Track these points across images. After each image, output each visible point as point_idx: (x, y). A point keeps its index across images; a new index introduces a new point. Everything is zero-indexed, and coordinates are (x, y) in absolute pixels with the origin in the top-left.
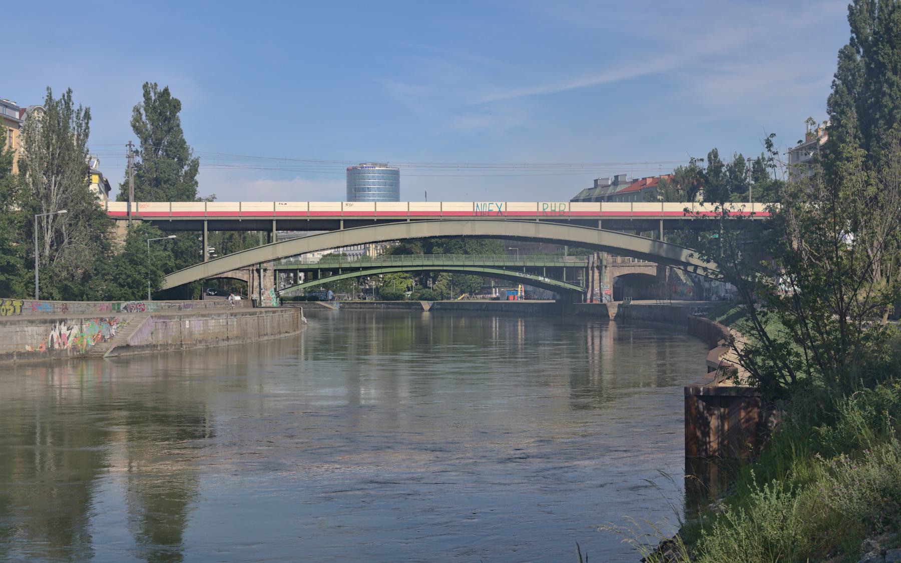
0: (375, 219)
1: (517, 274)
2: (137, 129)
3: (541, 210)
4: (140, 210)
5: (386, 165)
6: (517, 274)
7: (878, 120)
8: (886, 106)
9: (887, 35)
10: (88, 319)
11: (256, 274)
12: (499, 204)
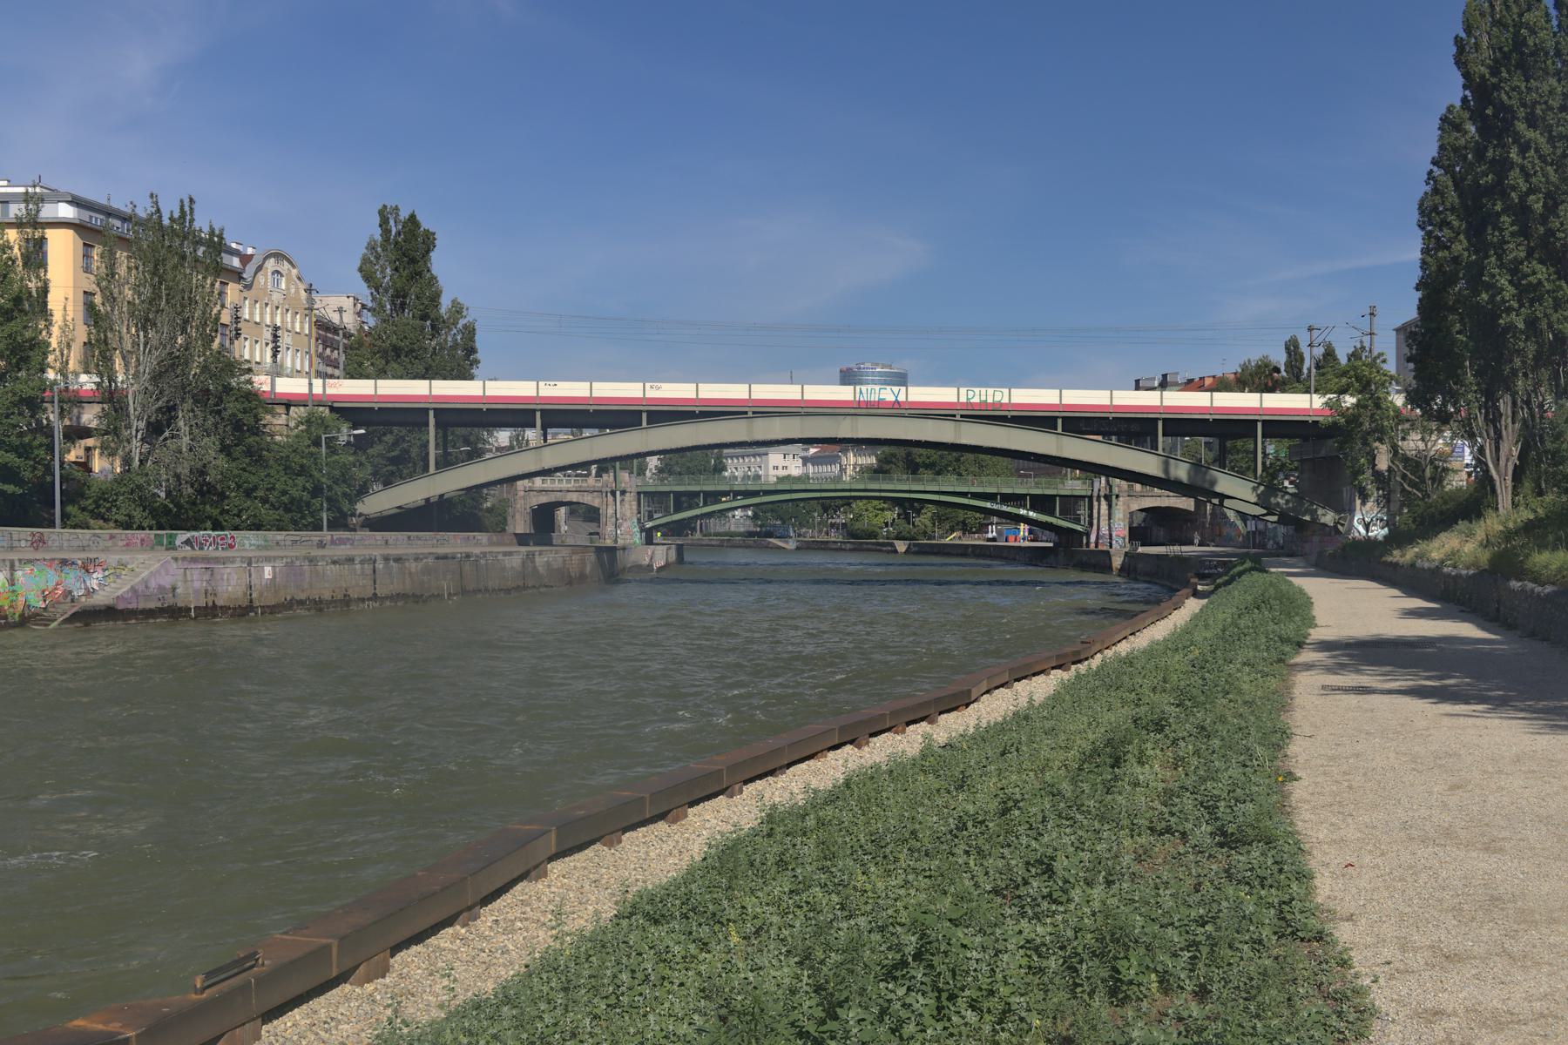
0: (697, 410)
1: (988, 505)
2: (368, 277)
3: (963, 399)
4: (329, 391)
5: (890, 366)
6: (988, 505)
7: (1498, 215)
8: (1514, 188)
9: (1518, 55)
10: (30, 561)
11: (610, 498)
12: (896, 389)
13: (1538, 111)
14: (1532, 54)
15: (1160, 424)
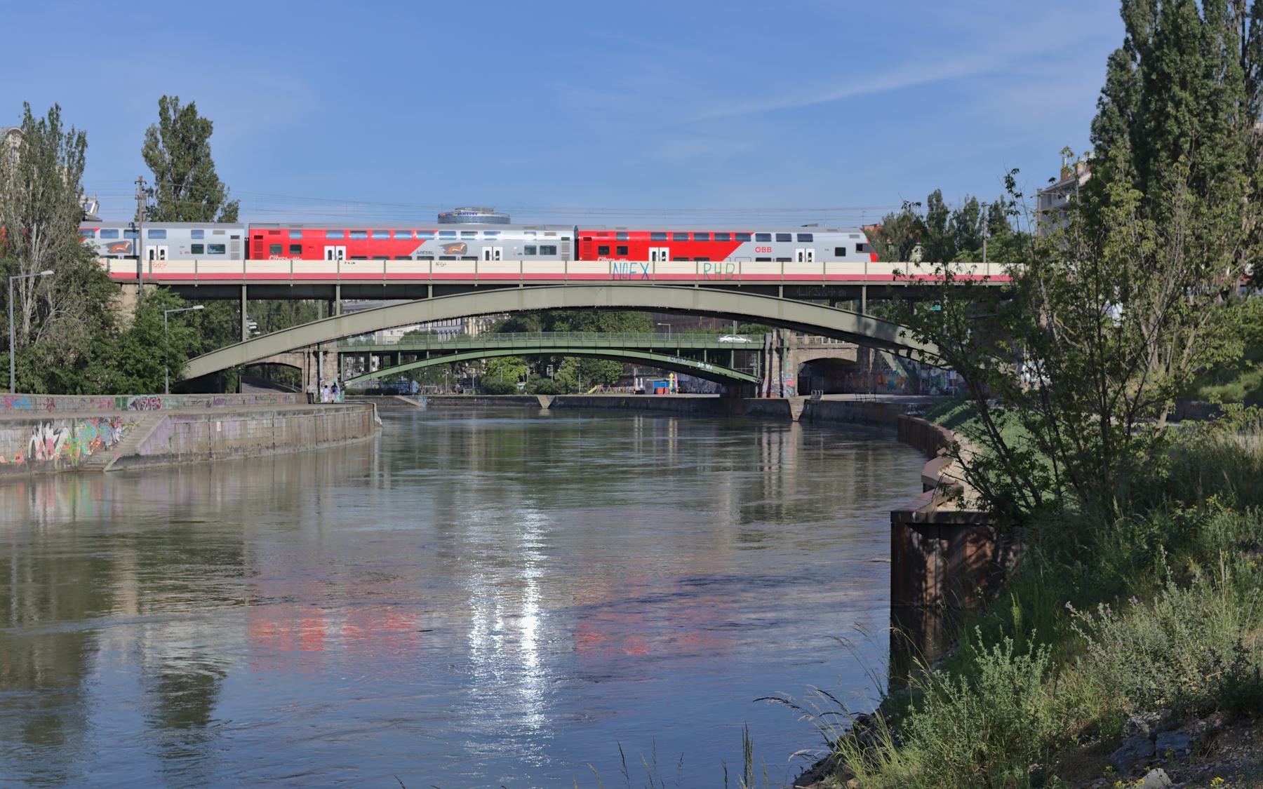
0: (476, 283)
1: (668, 359)
2: (151, 161)
3: (701, 272)
5: (491, 211)
6: (668, 359)
7: (1158, 151)
10: (83, 420)
11: (313, 359)
13: (1188, 78)
14: (1186, 37)
15: (864, 290)
